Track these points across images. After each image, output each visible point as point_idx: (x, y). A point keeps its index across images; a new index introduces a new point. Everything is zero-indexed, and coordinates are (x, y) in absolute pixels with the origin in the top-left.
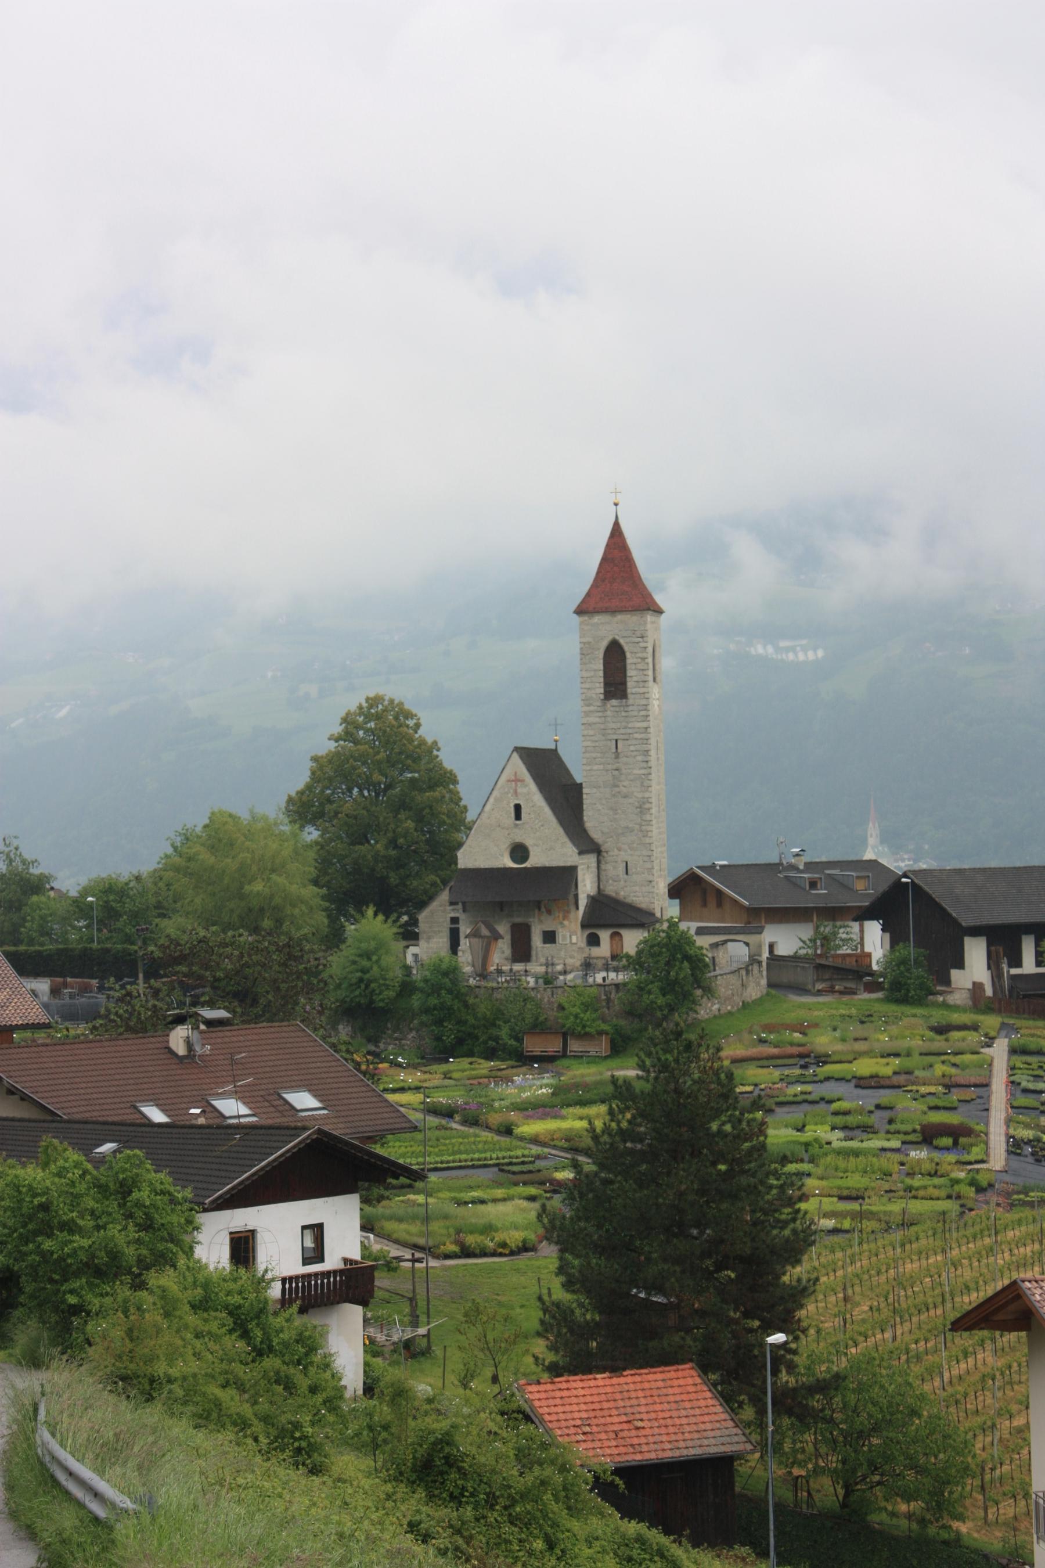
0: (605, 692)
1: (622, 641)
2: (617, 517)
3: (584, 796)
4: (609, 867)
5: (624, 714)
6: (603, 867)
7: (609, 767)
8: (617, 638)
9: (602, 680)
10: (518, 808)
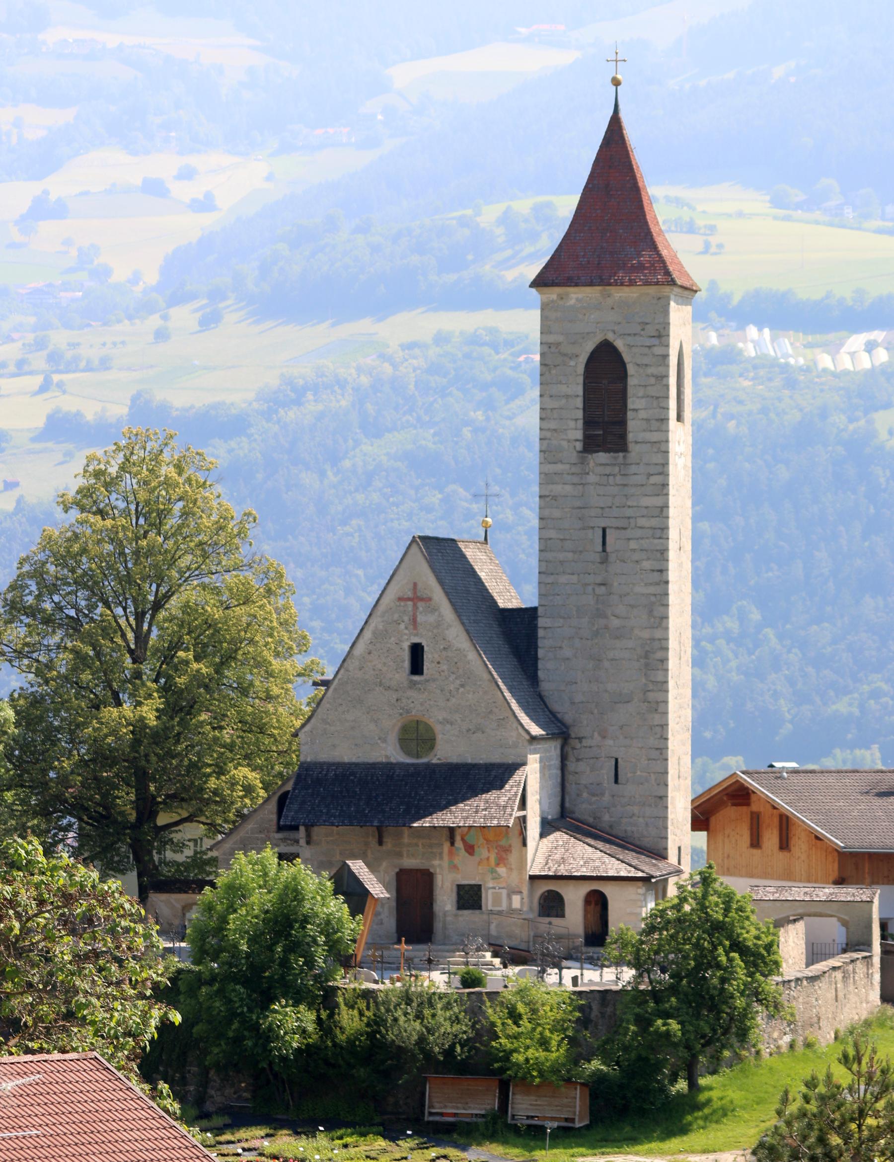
1: (619, 344)
4: (582, 766)
6: (571, 766)
8: (610, 337)
9: (580, 414)
10: (417, 651)
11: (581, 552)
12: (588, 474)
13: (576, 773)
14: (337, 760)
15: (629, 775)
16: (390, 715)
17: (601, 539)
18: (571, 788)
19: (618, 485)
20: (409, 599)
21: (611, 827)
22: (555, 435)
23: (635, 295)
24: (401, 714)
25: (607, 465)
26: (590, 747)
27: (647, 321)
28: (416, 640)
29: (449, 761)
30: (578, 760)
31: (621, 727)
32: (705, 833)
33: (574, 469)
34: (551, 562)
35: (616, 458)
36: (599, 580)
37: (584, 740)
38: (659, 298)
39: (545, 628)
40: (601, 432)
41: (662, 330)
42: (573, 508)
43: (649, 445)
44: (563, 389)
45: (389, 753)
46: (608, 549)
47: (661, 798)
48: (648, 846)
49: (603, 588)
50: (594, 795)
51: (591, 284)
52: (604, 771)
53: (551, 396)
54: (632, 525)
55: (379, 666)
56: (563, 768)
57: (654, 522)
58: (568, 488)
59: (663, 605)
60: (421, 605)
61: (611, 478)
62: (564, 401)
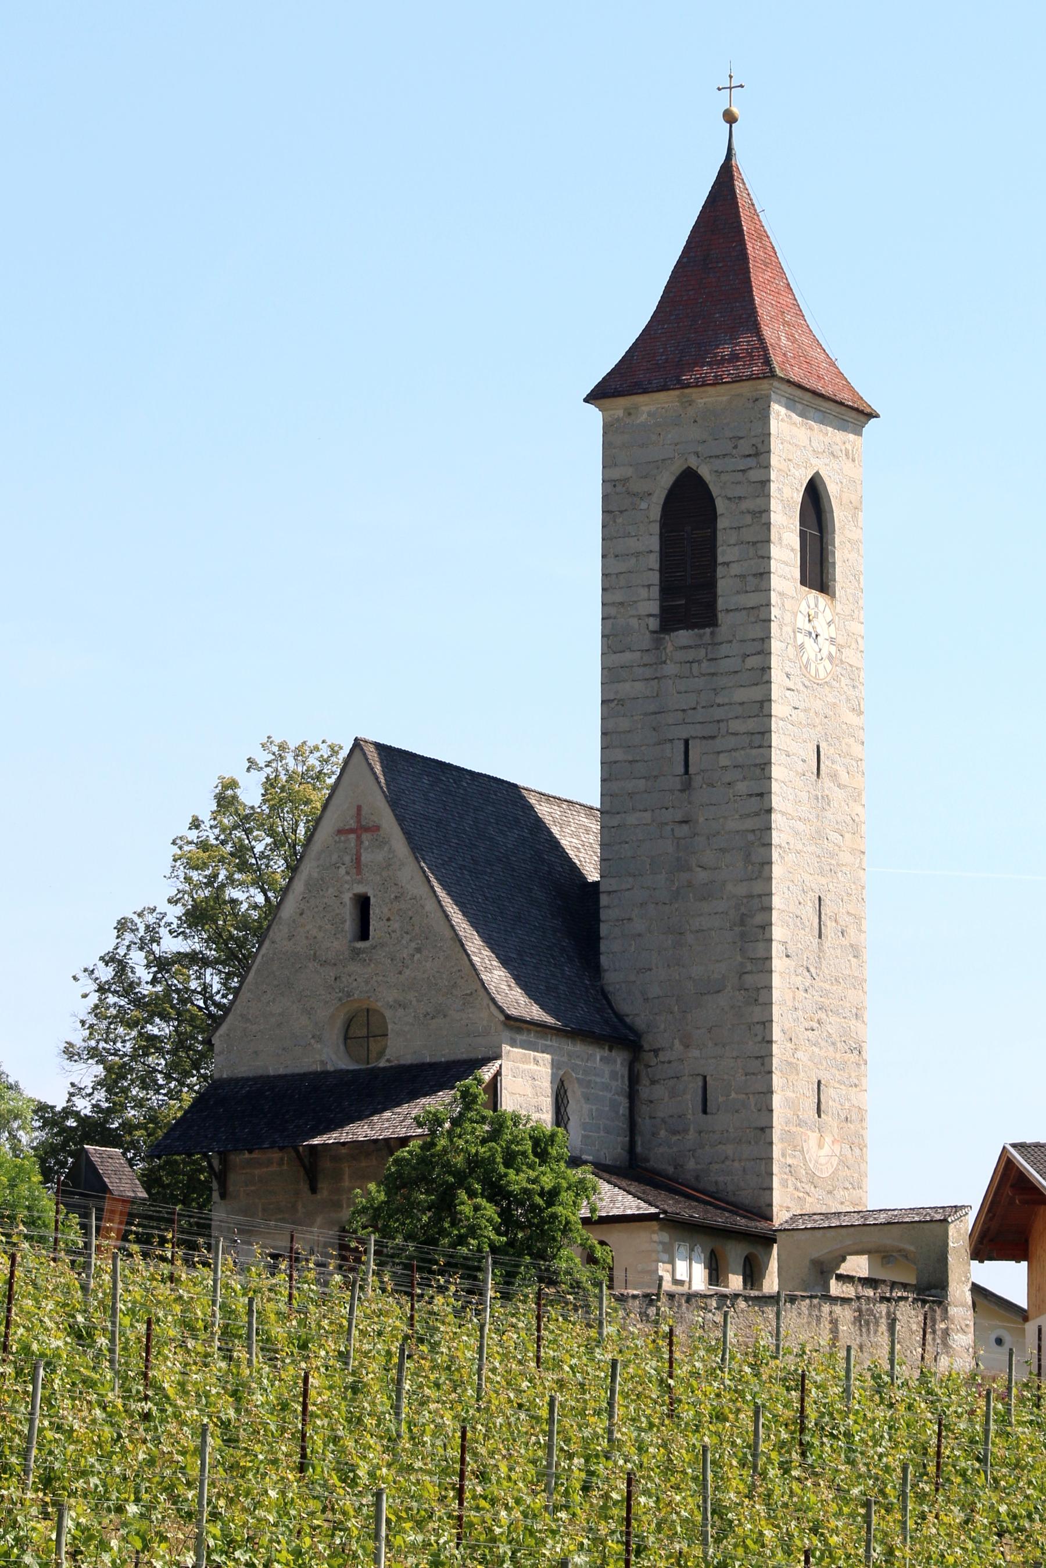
0: (663, 609)
1: (704, 472)
2: (730, 149)
4: (660, 1092)
6: (645, 1091)
8: (693, 462)
9: (655, 578)
10: (363, 904)
11: (656, 777)
12: (665, 662)
13: (651, 1102)
14: (260, 1072)
15: (721, 1099)
16: (326, 1002)
17: (682, 757)
18: (644, 1124)
19: (704, 675)
20: (351, 831)
21: (697, 1178)
22: (622, 610)
23: (724, 398)
24: (340, 1000)
25: (691, 647)
26: (670, 1062)
27: (740, 435)
28: (360, 889)
29: (402, 1062)
30: (653, 1082)
31: (710, 1030)
32: (1026, 1263)
33: (647, 659)
34: (617, 795)
35: (701, 636)
36: (679, 817)
37: (661, 1053)
38: (757, 400)
39: (609, 893)
40: (683, 602)
41: (759, 446)
42: (645, 714)
43: (744, 612)
44: (633, 544)
45: (324, 1057)
46: (691, 770)
47: (762, 1129)
48: (747, 1202)
49: (685, 827)
50: (675, 1132)
51: (664, 388)
52: (689, 1097)
53: (617, 556)
54: (723, 731)
55: (314, 932)
56: (632, 1095)
57: (751, 725)
58: (639, 686)
59: (764, 845)
60: (366, 837)
61: (695, 665)
62: (633, 560)
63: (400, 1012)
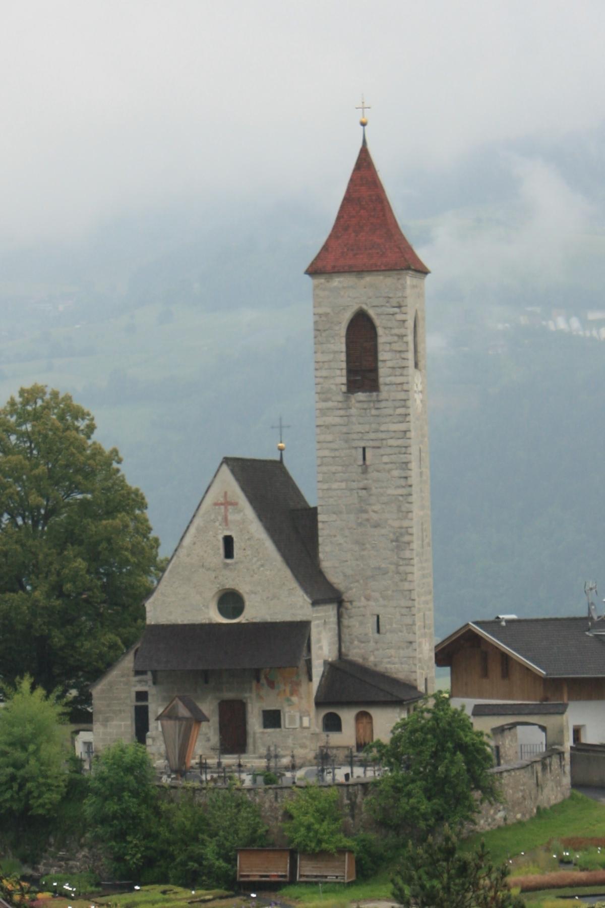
0: (348, 380)
1: (372, 312)
3: (320, 525)
5: (374, 412)
6: (345, 622)
7: (354, 485)
8: (365, 307)
9: (344, 365)
10: (228, 542)
18: (346, 638)
20: (222, 504)
28: (228, 533)
30: (350, 617)
35: (371, 396)
46: (368, 462)
60: (230, 507)
63: (253, 596)
